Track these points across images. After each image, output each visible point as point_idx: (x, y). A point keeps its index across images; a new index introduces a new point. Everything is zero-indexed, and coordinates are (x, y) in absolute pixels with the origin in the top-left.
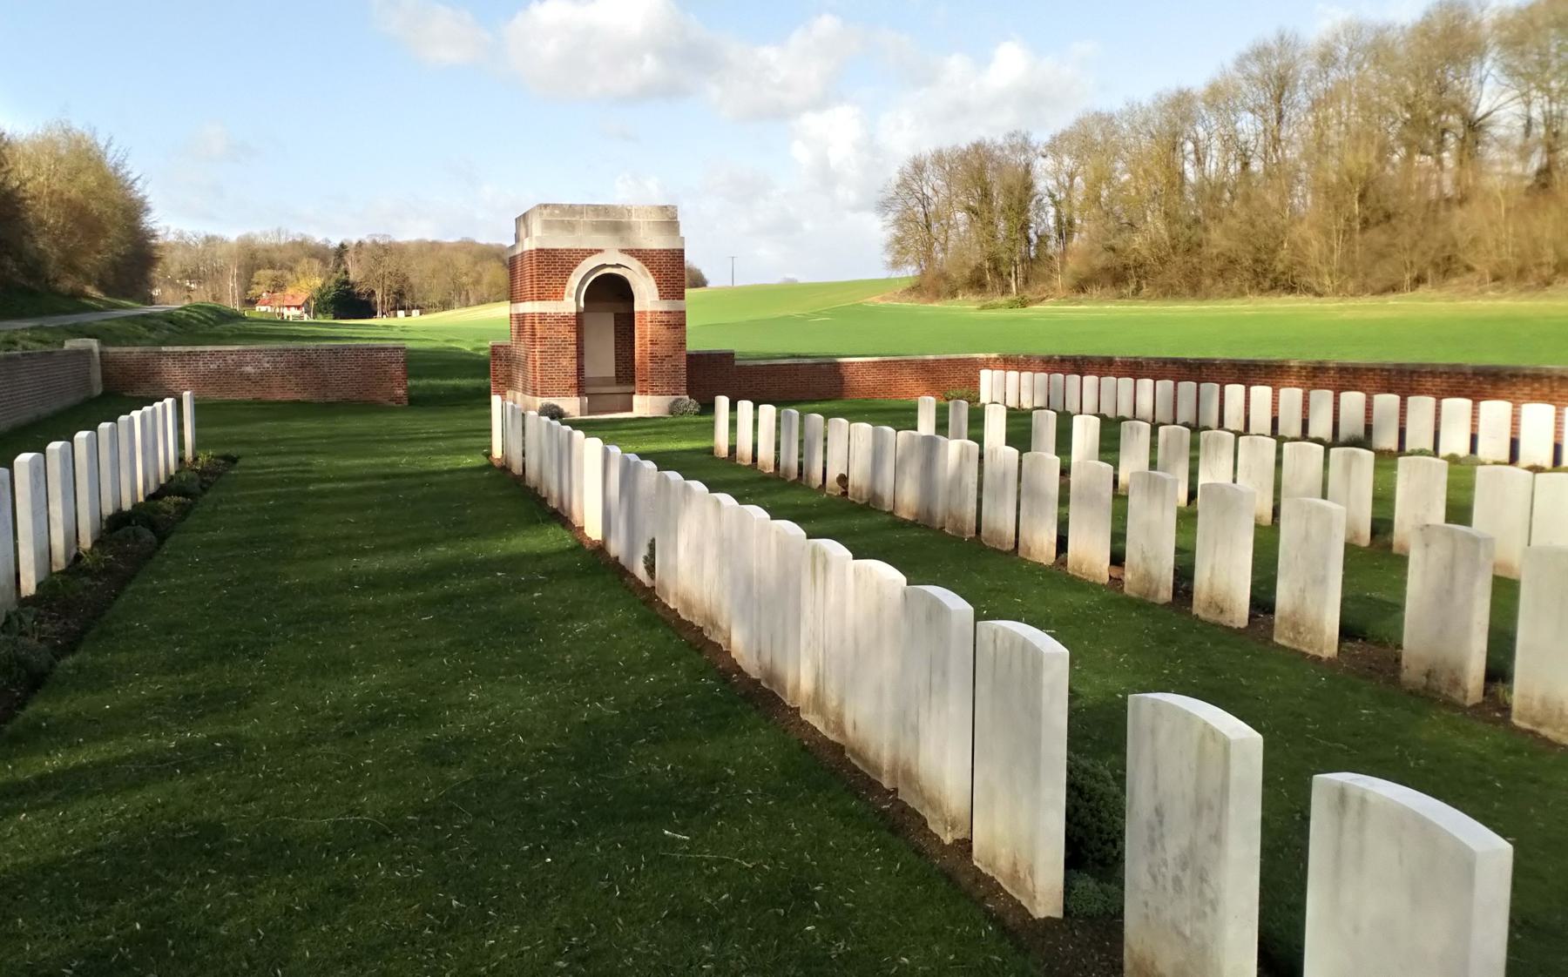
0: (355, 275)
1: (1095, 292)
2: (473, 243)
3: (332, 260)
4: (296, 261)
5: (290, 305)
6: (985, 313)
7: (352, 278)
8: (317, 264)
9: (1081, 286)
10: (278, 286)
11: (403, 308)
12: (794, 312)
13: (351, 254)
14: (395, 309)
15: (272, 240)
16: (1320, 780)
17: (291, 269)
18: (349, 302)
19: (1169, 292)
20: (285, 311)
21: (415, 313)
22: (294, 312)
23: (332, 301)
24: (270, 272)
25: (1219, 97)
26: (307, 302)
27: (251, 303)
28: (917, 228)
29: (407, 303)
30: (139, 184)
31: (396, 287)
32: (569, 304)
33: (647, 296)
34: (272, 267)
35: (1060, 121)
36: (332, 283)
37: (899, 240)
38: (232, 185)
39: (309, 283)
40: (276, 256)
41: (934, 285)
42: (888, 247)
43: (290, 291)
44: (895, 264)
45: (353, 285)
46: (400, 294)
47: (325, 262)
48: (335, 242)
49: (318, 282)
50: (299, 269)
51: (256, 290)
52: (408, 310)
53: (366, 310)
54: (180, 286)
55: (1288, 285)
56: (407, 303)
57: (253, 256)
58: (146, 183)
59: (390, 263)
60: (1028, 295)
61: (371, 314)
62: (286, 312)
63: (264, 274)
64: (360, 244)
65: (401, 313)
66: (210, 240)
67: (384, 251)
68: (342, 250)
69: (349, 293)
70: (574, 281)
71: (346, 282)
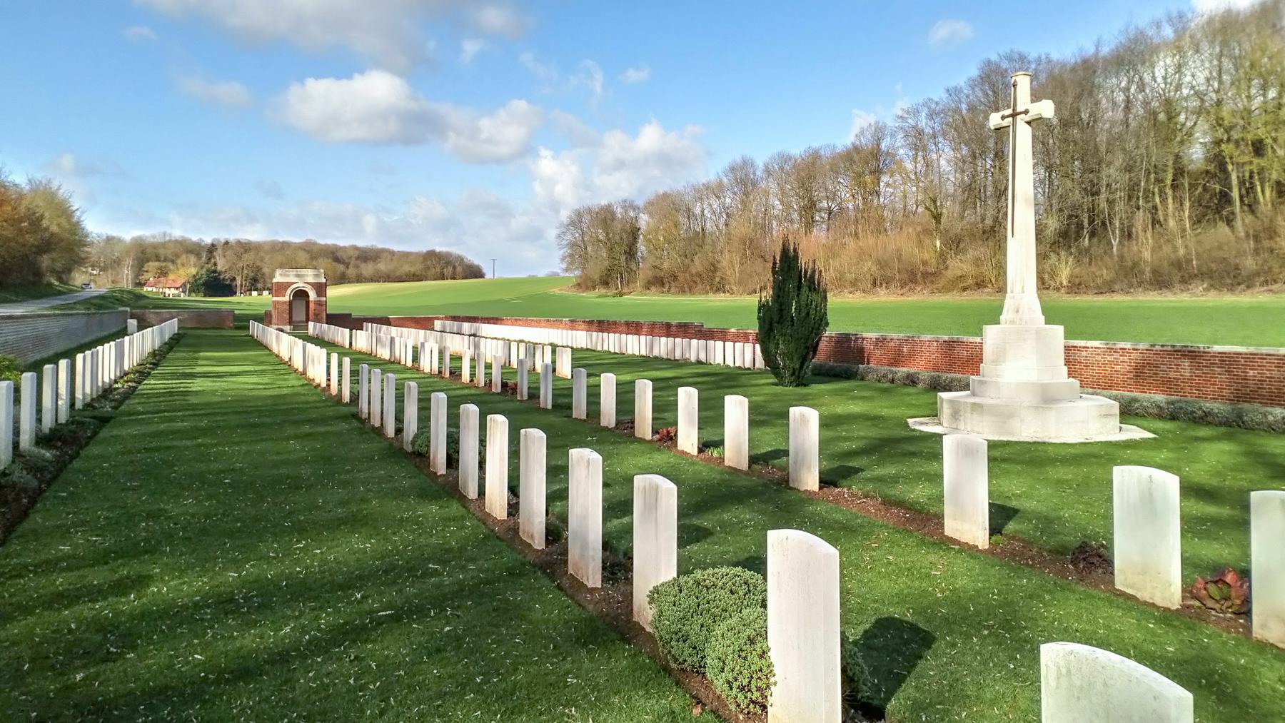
3: (204, 255)
4: (178, 256)
5: (170, 287)
6: (600, 300)
7: (219, 268)
8: (193, 259)
9: (648, 285)
10: (163, 273)
11: (256, 290)
12: (505, 297)
13: (220, 251)
17: (173, 262)
18: (216, 285)
20: (167, 291)
21: (265, 293)
22: (173, 291)
23: (204, 284)
24: (157, 264)
26: (184, 285)
27: (141, 285)
29: (259, 286)
30: (78, 213)
33: (312, 295)
35: (649, 194)
36: (204, 271)
37: (571, 256)
40: (162, 252)
41: (585, 284)
42: (563, 260)
43: (171, 277)
44: (567, 270)
46: (255, 280)
47: (198, 256)
48: (208, 240)
49: (193, 271)
50: (179, 261)
51: (146, 276)
52: (260, 291)
53: (228, 290)
54: (768, 414)
55: (720, 288)
56: (259, 286)
57: (143, 252)
58: (83, 212)
59: (249, 258)
61: (233, 293)
62: (167, 291)
63: (152, 266)
65: (255, 293)
66: (109, 240)
68: (212, 249)
69: (216, 279)
70: (289, 291)
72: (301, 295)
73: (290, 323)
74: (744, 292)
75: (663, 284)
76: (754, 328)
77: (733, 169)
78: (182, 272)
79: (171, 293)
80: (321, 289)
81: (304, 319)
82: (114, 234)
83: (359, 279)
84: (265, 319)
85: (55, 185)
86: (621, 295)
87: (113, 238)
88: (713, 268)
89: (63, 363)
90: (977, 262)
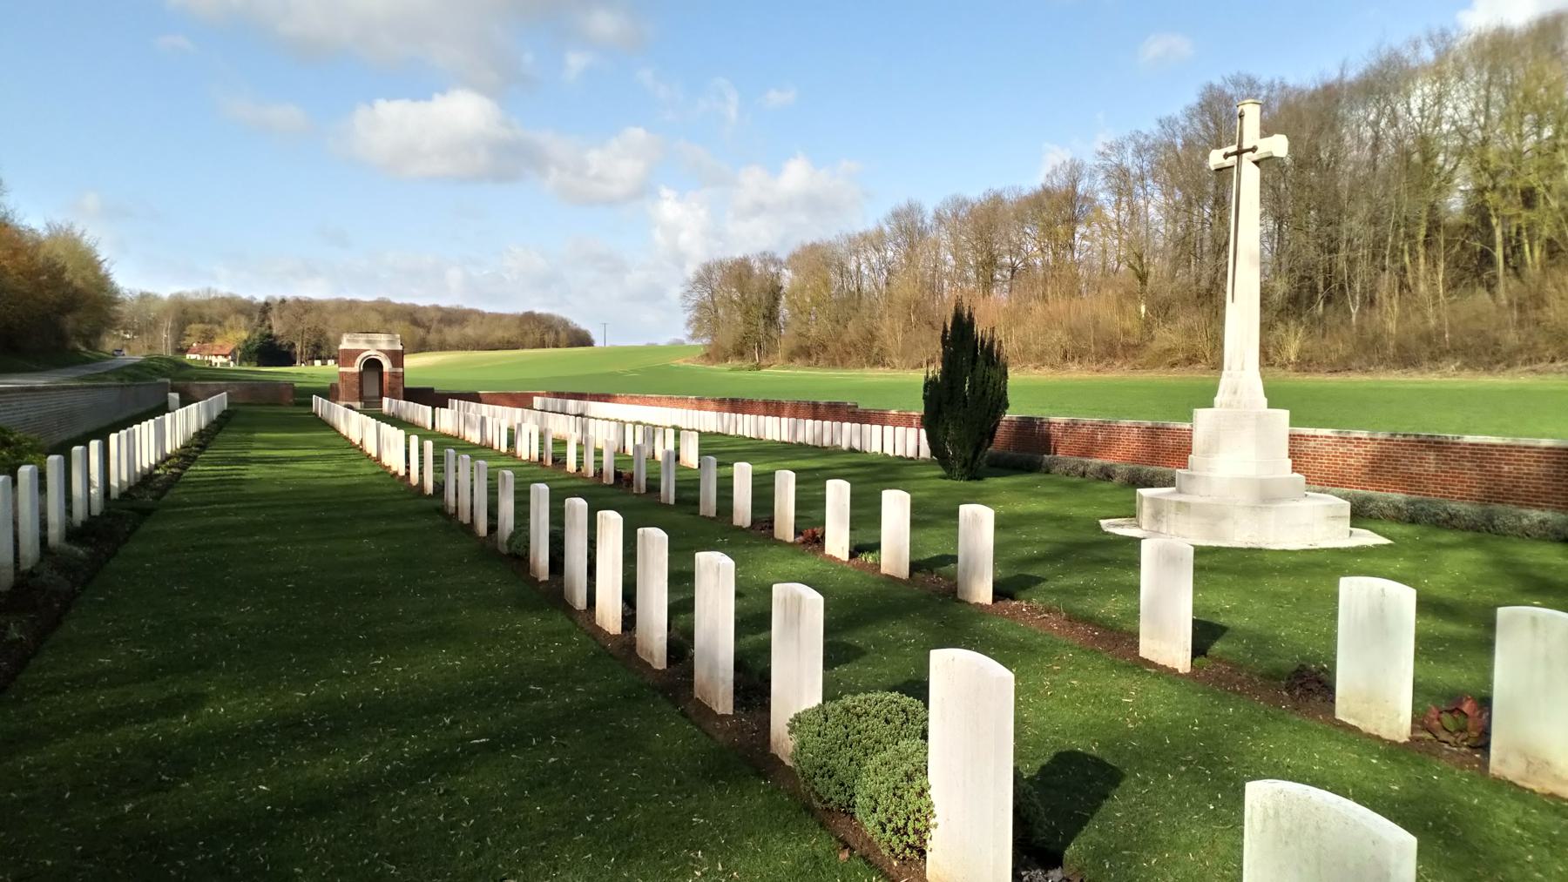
0: (278, 328)
1: (798, 361)
2: (389, 303)
3: (257, 315)
4: (225, 317)
6: (733, 374)
7: (275, 332)
8: (243, 320)
9: (791, 357)
10: (208, 337)
13: (275, 311)
14: (312, 359)
15: (203, 297)
16: (640, 531)
17: (220, 324)
18: (272, 352)
19: (833, 364)
20: (214, 359)
21: (331, 362)
22: (221, 359)
23: (257, 351)
24: (201, 326)
25: (875, 241)
27: (183, 351)
28: (706, 317)
30: (106, 265)
31: (314, 340)
32: (356, 368)
33: (387, 366)
34: (202, 322)
36: (256, 336)
37: (698, 320)
38: (168, 247)
39: (238, 334)
40: (206, 311)
41: (715, 355)
42: (688, 324)
43: (218, 342)
44: (693, 337)
45: (276, 338)
46: (318, 347)
47: (250, 316)
48: (261, 298)
49: (244, 335)
50: (227, 323)
51: (188, 341)
52: (324, 360)
53: (289, 360)
56: (323, 353)
57: (184, 312)
58: (112, 264)
59: (310, 320)
60: (764, 362)
61: (292, 362)
62: (214, 359)
63: (195, 328)
64: (283, 301)
65: (318, 363)
66: (144, 297)
67: (305, 307)
68: (266, 308)
69: (271, 345)
70: (359, 360)
71: (270, 336)
72: (373, 365)
73: (361, 399)
74: (907, 366)
75: (809, 356)
76: (918, 410)
77: (896, 215)
78: (230, 336)
79: (218, 361)
80: (397, 358)
81: (377, 393)
82: (150, 290)
83: (443, 347)
84: (330, 393)
85: (77, 230)
86: (759, 368)
87: (148, 295)
88: (871, 336)
89: (95, 445)
90: (1189, 332)
